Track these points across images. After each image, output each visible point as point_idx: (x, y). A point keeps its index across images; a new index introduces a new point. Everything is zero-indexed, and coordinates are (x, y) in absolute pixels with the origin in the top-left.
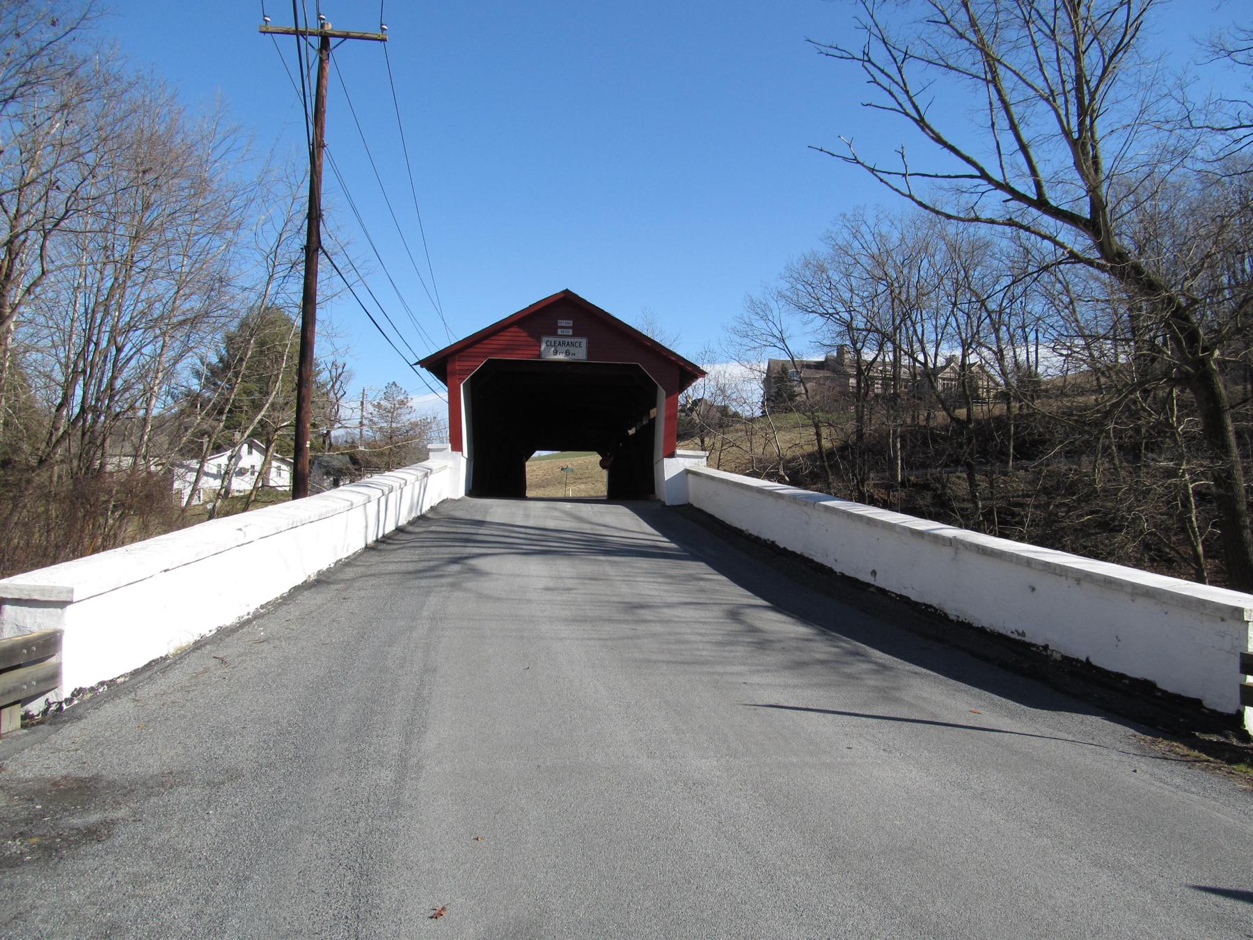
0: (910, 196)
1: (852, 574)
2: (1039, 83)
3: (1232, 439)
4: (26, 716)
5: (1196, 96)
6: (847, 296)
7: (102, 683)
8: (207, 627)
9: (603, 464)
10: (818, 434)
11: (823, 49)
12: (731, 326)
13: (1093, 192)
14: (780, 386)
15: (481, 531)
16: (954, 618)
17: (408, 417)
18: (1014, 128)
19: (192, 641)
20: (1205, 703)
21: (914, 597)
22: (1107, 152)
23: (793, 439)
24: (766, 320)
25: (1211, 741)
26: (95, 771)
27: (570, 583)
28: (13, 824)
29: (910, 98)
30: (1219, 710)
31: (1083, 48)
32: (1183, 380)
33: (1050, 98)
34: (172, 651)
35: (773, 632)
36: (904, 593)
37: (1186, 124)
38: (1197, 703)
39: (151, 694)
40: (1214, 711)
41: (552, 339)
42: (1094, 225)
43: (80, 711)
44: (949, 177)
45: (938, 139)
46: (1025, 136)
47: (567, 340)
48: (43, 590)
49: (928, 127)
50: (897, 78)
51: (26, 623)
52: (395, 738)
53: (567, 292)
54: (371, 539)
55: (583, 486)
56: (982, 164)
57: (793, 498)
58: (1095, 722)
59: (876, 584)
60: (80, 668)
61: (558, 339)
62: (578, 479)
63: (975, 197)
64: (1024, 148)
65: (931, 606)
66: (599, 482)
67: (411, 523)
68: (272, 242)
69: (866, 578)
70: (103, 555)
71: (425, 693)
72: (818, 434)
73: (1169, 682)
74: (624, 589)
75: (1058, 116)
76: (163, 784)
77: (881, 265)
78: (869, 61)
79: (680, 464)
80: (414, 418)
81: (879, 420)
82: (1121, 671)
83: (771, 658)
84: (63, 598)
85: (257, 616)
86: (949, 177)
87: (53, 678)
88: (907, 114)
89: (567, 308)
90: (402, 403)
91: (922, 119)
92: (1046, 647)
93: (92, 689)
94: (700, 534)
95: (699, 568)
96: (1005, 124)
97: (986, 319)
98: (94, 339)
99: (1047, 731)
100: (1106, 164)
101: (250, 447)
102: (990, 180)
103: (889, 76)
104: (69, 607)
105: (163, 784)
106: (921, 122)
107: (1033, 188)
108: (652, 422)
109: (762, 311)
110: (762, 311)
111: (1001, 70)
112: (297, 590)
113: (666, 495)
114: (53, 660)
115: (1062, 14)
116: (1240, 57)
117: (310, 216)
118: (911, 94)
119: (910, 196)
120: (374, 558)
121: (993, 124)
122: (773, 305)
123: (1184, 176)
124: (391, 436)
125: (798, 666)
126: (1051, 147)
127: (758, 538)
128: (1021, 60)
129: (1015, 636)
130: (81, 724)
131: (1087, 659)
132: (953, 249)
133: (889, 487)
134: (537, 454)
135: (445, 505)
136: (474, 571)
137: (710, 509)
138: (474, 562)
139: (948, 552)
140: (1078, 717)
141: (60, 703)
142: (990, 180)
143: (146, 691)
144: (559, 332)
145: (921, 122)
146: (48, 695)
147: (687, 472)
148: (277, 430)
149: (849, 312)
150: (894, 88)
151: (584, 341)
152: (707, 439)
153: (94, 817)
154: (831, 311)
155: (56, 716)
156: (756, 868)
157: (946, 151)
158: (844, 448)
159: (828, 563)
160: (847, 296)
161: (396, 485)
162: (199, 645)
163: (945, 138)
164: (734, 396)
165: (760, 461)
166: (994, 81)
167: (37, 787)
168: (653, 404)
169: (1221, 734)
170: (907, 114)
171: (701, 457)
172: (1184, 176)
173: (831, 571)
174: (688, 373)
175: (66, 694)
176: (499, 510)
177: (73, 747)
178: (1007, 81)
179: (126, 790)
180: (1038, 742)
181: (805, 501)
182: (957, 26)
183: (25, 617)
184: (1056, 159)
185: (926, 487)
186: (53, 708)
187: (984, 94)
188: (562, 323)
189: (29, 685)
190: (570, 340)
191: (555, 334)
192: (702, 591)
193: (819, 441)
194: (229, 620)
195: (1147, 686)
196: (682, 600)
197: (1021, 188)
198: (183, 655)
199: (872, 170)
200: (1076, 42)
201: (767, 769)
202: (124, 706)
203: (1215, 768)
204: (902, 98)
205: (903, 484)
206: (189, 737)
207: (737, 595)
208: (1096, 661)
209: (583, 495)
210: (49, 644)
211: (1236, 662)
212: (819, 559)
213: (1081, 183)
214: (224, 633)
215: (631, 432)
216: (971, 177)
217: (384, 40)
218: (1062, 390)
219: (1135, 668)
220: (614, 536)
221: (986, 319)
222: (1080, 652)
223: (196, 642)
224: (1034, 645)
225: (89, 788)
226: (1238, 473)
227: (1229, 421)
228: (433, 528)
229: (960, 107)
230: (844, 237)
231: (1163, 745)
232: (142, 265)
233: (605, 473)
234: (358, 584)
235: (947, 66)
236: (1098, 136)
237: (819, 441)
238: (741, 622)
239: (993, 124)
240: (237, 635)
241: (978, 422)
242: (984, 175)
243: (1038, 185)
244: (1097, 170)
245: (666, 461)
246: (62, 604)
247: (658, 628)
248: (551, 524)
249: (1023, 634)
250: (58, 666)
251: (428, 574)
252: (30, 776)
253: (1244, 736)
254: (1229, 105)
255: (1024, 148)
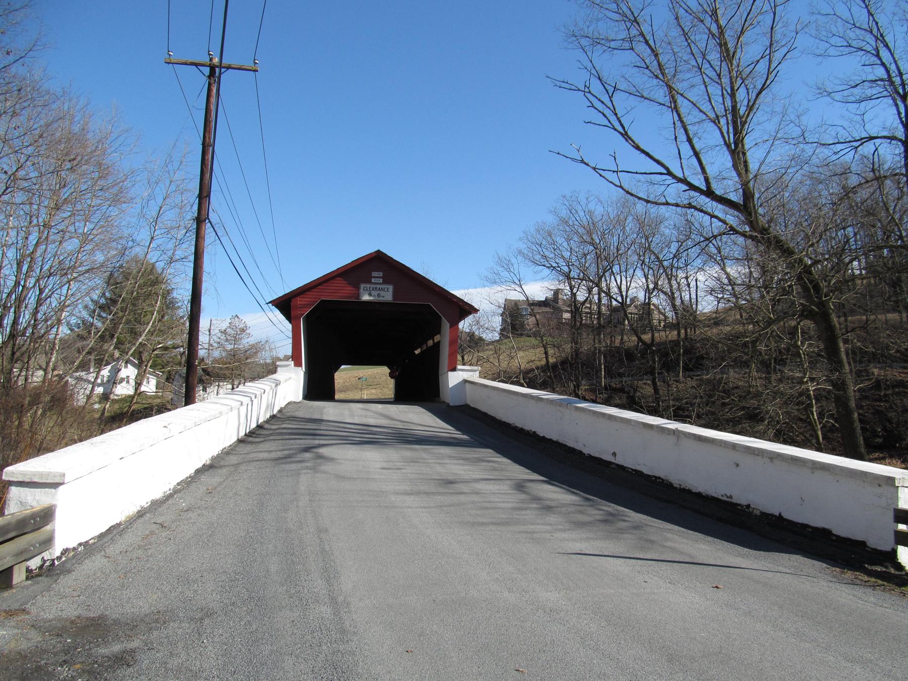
0: (621, 187)
1: (597, 455)
2: (706, 107)
3: (844, 356)
4: (29, 571)
5: (810, 121)
6: (567, 254)
7: (80, 544)
8: (144, 501)
9: (391, 375)
10: (546, 353)
11: (558, 83)
12: (489, 275)
13: (745, 185)
14: (514, 318)
15: (322, 428)
16: (678, 486)
17: (246, 341)
18: (689, 140)
19: (136, 511)
20: (868, 544)
21: (646, 471)
22: (754, 158)
23: (528, 356)
24: (509, 271)
25: (876, 571)
26: (100, 613)
27: (399, 464)
28: (55, 654)
29: (618, 119)
30: (879, 548)
31: (736, 88)
32: (806, 314)
33: (716, 121)
34: (123, 519)
35: (552, 500)
36: (638, 468)
37: (801, 139)
38: (863, 544)
39: (117, 552)
40: (875, 550)
41: (368, 286)
42: (745, 207)
43: (68, 566)
44: (645, 173)
45: (637, 148)
46: (697, 148)
47: (378, 286)
48: (41, 475)
49: (630, 139)
50: (609, 104)
51: (21, 502)
52: (319, 581)
53: (379, 252)
54: (242, 434)
55: (373, 391)
56: (667, 165)
57: (551, 402)
58: (797, 560)
59: (616, 462)
60: (69, 532)
61: (372, 286)
62: (369, 386)
63: (663, 188)
64: (696, 154)
65: (659, 478)
66: (388, 388)
67: (267, 422)
68: (155, 214)
69: (608, 457)
70: (79, 445)
71: (327, 548)
72: (546, 353)
73: (841, 529)
74: (439, 469)
75: (722, 133)
76: (157, 621)
77: (590, 233)
78: (590, 92)
79: (459, 377)
80: (252, 341)
81: (587, 344)
82: (805, 522)
83: (552, 518)
84: (57, 480)
85: (176, 491)
86: (645, 173)
87: (48, 542)
88: (615, 130)
89: (378, 263)
90: (243, 330)
91: (626, 133)
92: (748, 506)
93: (74, 549)
94: (480, 427)
95: (487, 453)
96: (684, 138)
97: (663, 269)
98: (22, 283)
99: (771, 567)
100: (753, 166)
101: (126, 363)
102: (674, 177)
103: (603, 103)
104: (61, 487)
105: (157, 621)
106: (625, 135)
107: (704, 184)
108: (437, 346)
109: (507, 265)
110: (507, 265)
111: (680, 100)
112: (198, 472)
113: (449, 397)
114: (48, 527)
115: (724, 64)
116: (837, 97)
117: (200, 197)
118: (619, 116)
119: (621, 187)
120: (248, 448)
121: (676, 138)
122: (514, 260)
123: (796, 177)
124: (233, 354)
125: (580, 525)
126: (714, 153)
127: (522, 430)
128: (696, 94)
129: (725, 498)
130: (73, 575)
131: (780, 514)
132: (641, 223)
133: (593, 391)
134: (343, 367)
135: (290, 406)
136: (320, 457)
137: (483, 409)
138: (322, 451)
139: (672, 439)
140: (786, 556)
141: (53, 560)
142: (674, 177)
143: (113, 550)
144: (373, 280)
145: (625, 135)
146: (43, 554)
147: (465, 381)
148: (154, 350)
149: (568, 266)
150: (608, 112)
151: (391, 287)
152: (466, 357)
153: (116, 648)
154: (554, 265)
155: (49, 570)
156: (622, 670)
157: (643, 155)
158: (564, 362)
159: (578, 446)
160: (567, 254)
161: (258, 393)
162: (141, 514)
163: (642, 147)
164: (486, 326)
165: (505, 372)
166: (676, 109)
167: (59, 625)
168: (438, 331)
169: (882, 566)
170: (615, 130)
171: (475, 371)
172: (796, 177)
173: (580, 452)
174: (465, 309)
175: (58, 553)
176: (327, 410)
177: (75, 594)
178: (684, 106)
179: (131, 626)
180: (770, 575)
181: (569, 403)
182: (653, 70)
183: (26, 495)
184: (719, 162)
185: (622, 390)
186: (48, 564)
187: (668, 117)
188: (375, 274)
189: (34, 546)
190: (383, 286)
191: (370, 282)
192: (495, 469)
193: (547, 358)
194: (158, 495)
195: (825, 533)
196: (482, 477)
197: (696, 183)
198: (132, 521)
199: (594, 169)
200: (732, 83)
201: (596, 599)
202: (97, 562)
203: (890, 590)
204: (613, 119)
205: (606, 388)
206: (163, 584)
207: (520, 472)
208: (786, 515)
209: (374, 397)
210: (47, 515)
211: (891, 515)
212: (571, 444)
213: (737, 179)
214: (156, 505)
215: (417, 352)
216: (661, 174)
217: (256, 71)
218: (716, 320)
219: (817, 521)
220: (420, 431)
221: (663, 269)
222: (773, 509)
223: (139, 512)
224: (739, 505)
225: (100, 625)
226: (849, 379)
227: (841, 344)
228: (284, 426)
229: (652, 126)
230: (564, 213)
231: (849, 575)
232: (60, 227)
233: (393, 381)
234: (243, 467)
235: (642, 97)
236: (746, 147)
237: (547, 358)
238: (525, 492)
239: (676, 138)
240: (165, 506)
241: (659, 344)
242: (669, 173)
243: (707, 180)
244: (747, 171)
245: (450, 374)
246: (55, 485)
247: (475, 498)
248: (372, 421)
249: (731, 497)
250: (53, 532)
251: (284, 461)
252: (51, 617)
253: (900, 567)
254: (830, 128)
255: (696, 154)
